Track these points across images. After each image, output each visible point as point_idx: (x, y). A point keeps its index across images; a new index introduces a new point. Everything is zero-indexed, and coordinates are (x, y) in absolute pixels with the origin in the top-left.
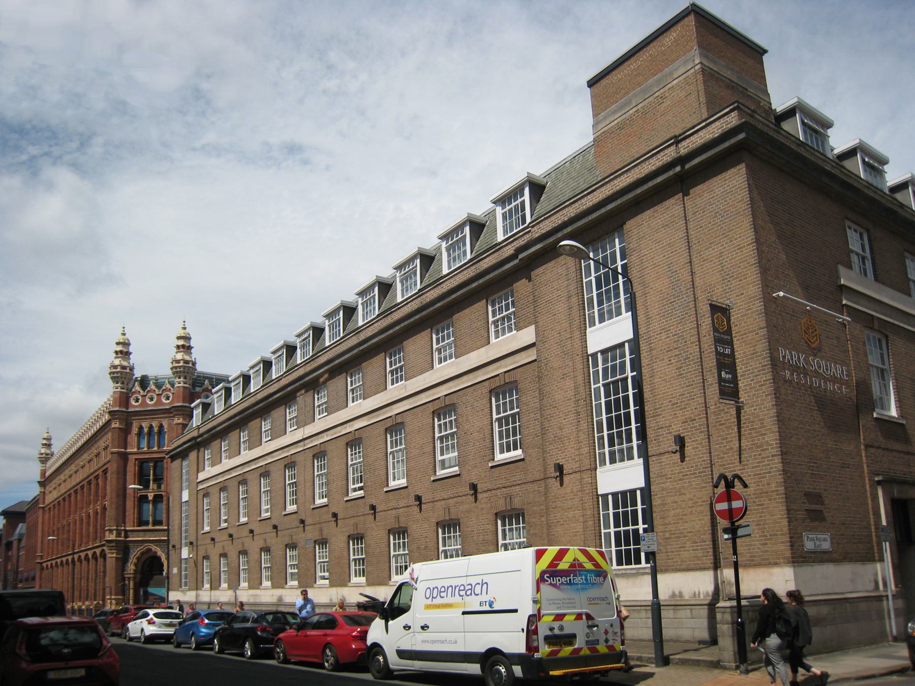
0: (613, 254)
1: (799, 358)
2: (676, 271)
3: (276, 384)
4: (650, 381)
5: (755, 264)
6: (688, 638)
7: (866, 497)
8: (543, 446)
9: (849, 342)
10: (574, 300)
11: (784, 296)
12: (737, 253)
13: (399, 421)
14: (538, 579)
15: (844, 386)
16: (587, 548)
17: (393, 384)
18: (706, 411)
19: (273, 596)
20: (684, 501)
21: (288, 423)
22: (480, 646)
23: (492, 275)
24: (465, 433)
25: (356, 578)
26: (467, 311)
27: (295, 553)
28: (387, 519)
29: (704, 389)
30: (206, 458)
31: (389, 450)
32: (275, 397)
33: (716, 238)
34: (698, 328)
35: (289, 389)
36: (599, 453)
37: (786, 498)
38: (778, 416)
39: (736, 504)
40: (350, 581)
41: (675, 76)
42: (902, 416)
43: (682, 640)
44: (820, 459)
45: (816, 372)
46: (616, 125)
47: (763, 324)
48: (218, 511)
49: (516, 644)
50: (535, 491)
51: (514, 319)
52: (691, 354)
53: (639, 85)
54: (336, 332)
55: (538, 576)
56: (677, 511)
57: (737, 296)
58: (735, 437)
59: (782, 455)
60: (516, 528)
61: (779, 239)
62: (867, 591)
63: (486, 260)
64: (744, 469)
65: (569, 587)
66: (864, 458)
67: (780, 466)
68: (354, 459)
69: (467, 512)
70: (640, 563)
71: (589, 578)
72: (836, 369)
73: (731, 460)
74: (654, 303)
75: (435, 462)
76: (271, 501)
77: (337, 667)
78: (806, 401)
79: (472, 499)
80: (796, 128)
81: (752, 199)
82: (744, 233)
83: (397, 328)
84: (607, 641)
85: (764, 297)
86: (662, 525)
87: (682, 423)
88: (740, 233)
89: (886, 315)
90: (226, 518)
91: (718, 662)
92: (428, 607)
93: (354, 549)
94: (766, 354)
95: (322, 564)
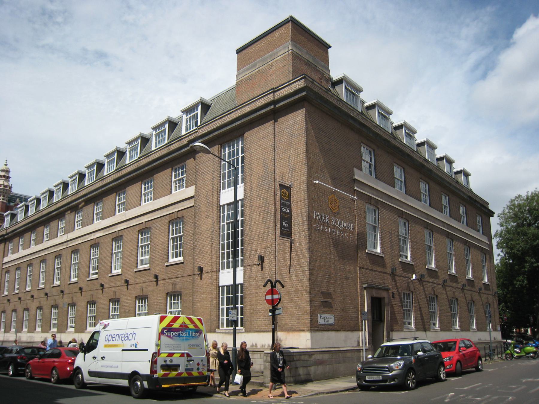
0: (238, 150)
1: (325, 217)
2: (267, 163)
3: (54, 206)
4: (249, 223)
5: (305, 164)
6: (258, 370)
7: (358, 296)
8: (193, 256)
9: (356, 210)
10: (216, 174)
11: (318, 183)
12: (297, 157)
13: (120, 234)
14: (160, 333)
15: (350, 235)
16: (191, 317)
17: (119, 212)
18: (275, 243)
19: (41, 337)
20: (261, 292)
21: (60, 231)
22: (128, 370)
23: (175, 154)
24: (154, 245)
26: (161, 173)
27: (56, 311)
28: (109, 293)
29: (275, 231)
30: (10, 248)
31: (114, 252)
32: (53, 214)
33: (288, 147)
34: (275, 196)
35: (61, 209)
36: (222, 262)
37: (310, 294)
38: (309, 249)
39: (276, 297)
40: (86, 329)
41: (279, 55)
42: (382, 253)
43: (255, 371)
44: (333, 273)
45: (334, 225)
46: (248, 77)
47: (306, 198)
48: (14, 282)
49: (145, 369)
50: (188, 281)
51: (186, 181)
52: (270, 211)
53: (262, 56)
54: (92, 177)
55: (160, 331)
56: (257, 298)
57: (295, 181)
58: (288, 259)
59: (310, 270)
60: (177, 302)
61: (321, 152)
62: (353, 347)
63: (174, 145)
64: (291, 277)
65: (178, 338)
66: (358, 274)
67: (308, 276)
68: (94, 255)
69: (152, 291)
70: (224, 327)
71: (190, 333)
72: (347, 225)
73: (285, 271)
74: (255, 180)
75: (137, 261)
76: (46, 279)
77: (58, 381)
78: (327, 241)
79: (155, 284)
80: (341, 91)
81: (307, 128)
82: (301, 147)
83: (123, 179)
84: (198, 369)
85: (308, 183)
86: (249, 305)
87: (263, 249)
88: (300, 146)
89: (379, 197)
90: (18, 287)
91: (263, 383)
92: (106, 346)
93: (90, 310)
94: (306, 214)
95: (72, 318)
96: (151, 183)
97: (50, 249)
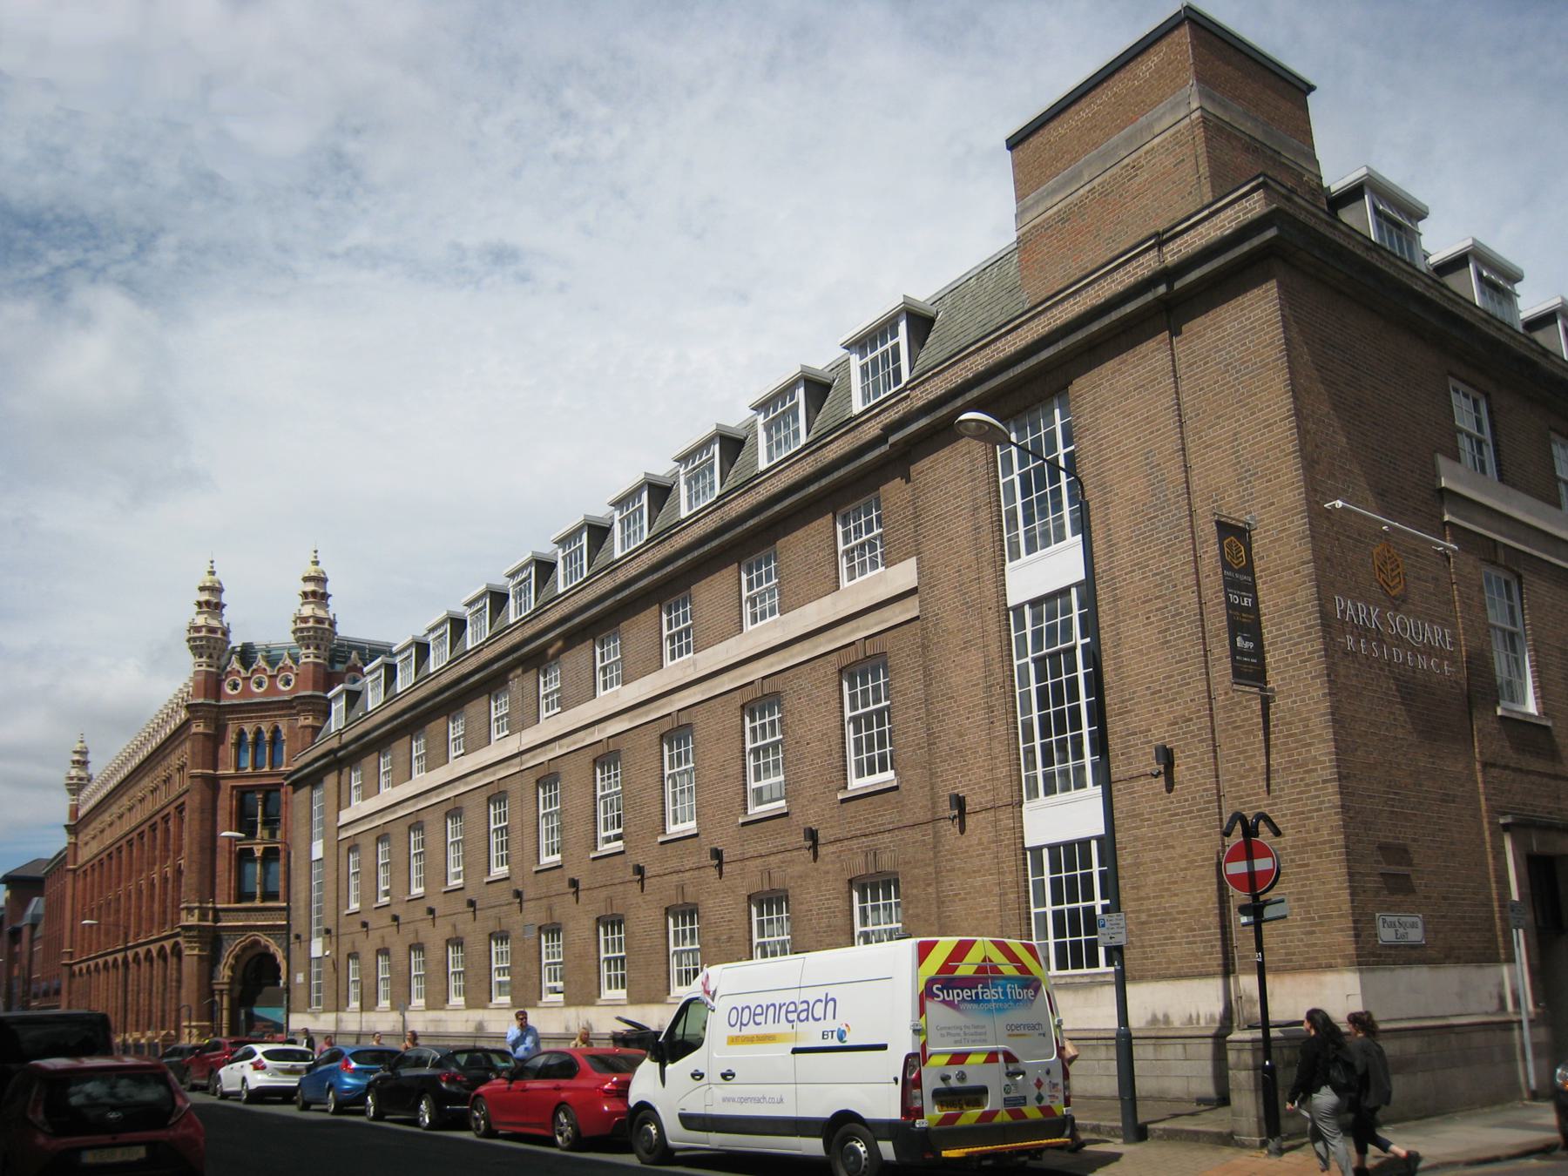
0: (1051, 436)
1: (1369, 613)
2: (1159, 465)
3: (473, 658)
4: (1114, 653)
5: (1294, 452)
6: (1180, 1094)
7: (1484, 852)
8: (930, 764)
9: (1455, 587)
10: (984, 514)
11: (1343, 507)
12: (1264, 434)
13: (684, 721)
14: (922, 992)
15: (1446, 663)
16: (1006, 940)
17: (673, 658)
18: (1211, 704)
19: (467, 1021)
20: (1173, 858)
21: (494, 726)
22: (822, 1108)
23: (842, 472)
24: (797, 743)
25: (610, 992)
26: (800, 533)
27: (505, 948)
28: (663, 890)
29: (1207, 668)
30: (353, 785)
31: (667, 772)
32: (472, 680)
33: (1227, 407)
34: (1196, 562)
35: (496, 666)
36: (1026, 776)
37: (1348, 854)
38: (1332, 714)
39: (1262, 864)
40: (599, 996)
41: (1157, 131)
42: (1545, 714)
43: (1169, 1097)
44: (1406, 786)
45: (1398, 637)
46: (1055, 214)
47: (1308, 556)
48: (374, 875)
49: (884, 1104)
50: (916, 842)
51: (881, 547)
52: (1184, 607)
53: (1096, 145)
54: (576, 569)
55: (922, 987)
56: (1160, 876)
57: (1263, 508)
58: (1259, 749)
59: (1340, 780)
60: (884, 905)
61: (1334, 410)
62: (1487, 1013)
63: (833, 446)
64: (1276, 804)
65: (975, 1006)
66: (1481, 785)
67: (1337, 799)
68: (607, 786)
69: (800, 877)
70: (1098, 966)
71: (1009, 990)
72: (1433, 632)
73: (1253, 788)
74: (1122, 519)
75: (746, 792)
76: (465, 859)
77: (578, 1143)
78: (1381, 687)
79: (809, 855)
80: (1363, 219)
81: (1288, 341)
82: (1274, 399)
83: (681, 562)
84: (1040, 1098)
85: (1310, 510)
86: (1135, 900)
87: (1169, 725)
88: (1268, 400)
89: (1518, 541)
90: (388, 887)
91: (1231, 1134)
92: (734, 1040)
93: (606, 941)
94: (1313, 606)
95: (552, 967)
96: (685, 606)
97: (525, 757)
